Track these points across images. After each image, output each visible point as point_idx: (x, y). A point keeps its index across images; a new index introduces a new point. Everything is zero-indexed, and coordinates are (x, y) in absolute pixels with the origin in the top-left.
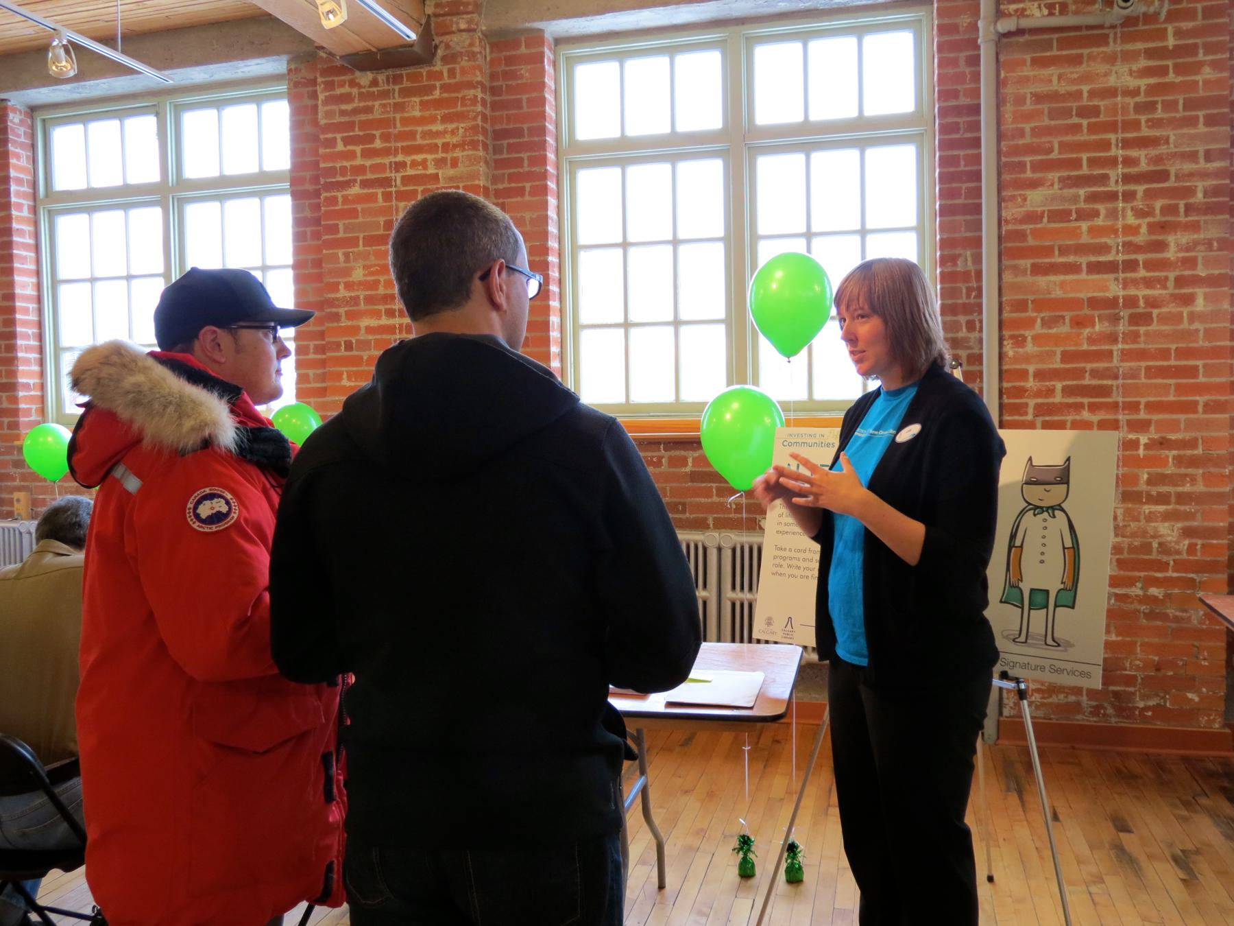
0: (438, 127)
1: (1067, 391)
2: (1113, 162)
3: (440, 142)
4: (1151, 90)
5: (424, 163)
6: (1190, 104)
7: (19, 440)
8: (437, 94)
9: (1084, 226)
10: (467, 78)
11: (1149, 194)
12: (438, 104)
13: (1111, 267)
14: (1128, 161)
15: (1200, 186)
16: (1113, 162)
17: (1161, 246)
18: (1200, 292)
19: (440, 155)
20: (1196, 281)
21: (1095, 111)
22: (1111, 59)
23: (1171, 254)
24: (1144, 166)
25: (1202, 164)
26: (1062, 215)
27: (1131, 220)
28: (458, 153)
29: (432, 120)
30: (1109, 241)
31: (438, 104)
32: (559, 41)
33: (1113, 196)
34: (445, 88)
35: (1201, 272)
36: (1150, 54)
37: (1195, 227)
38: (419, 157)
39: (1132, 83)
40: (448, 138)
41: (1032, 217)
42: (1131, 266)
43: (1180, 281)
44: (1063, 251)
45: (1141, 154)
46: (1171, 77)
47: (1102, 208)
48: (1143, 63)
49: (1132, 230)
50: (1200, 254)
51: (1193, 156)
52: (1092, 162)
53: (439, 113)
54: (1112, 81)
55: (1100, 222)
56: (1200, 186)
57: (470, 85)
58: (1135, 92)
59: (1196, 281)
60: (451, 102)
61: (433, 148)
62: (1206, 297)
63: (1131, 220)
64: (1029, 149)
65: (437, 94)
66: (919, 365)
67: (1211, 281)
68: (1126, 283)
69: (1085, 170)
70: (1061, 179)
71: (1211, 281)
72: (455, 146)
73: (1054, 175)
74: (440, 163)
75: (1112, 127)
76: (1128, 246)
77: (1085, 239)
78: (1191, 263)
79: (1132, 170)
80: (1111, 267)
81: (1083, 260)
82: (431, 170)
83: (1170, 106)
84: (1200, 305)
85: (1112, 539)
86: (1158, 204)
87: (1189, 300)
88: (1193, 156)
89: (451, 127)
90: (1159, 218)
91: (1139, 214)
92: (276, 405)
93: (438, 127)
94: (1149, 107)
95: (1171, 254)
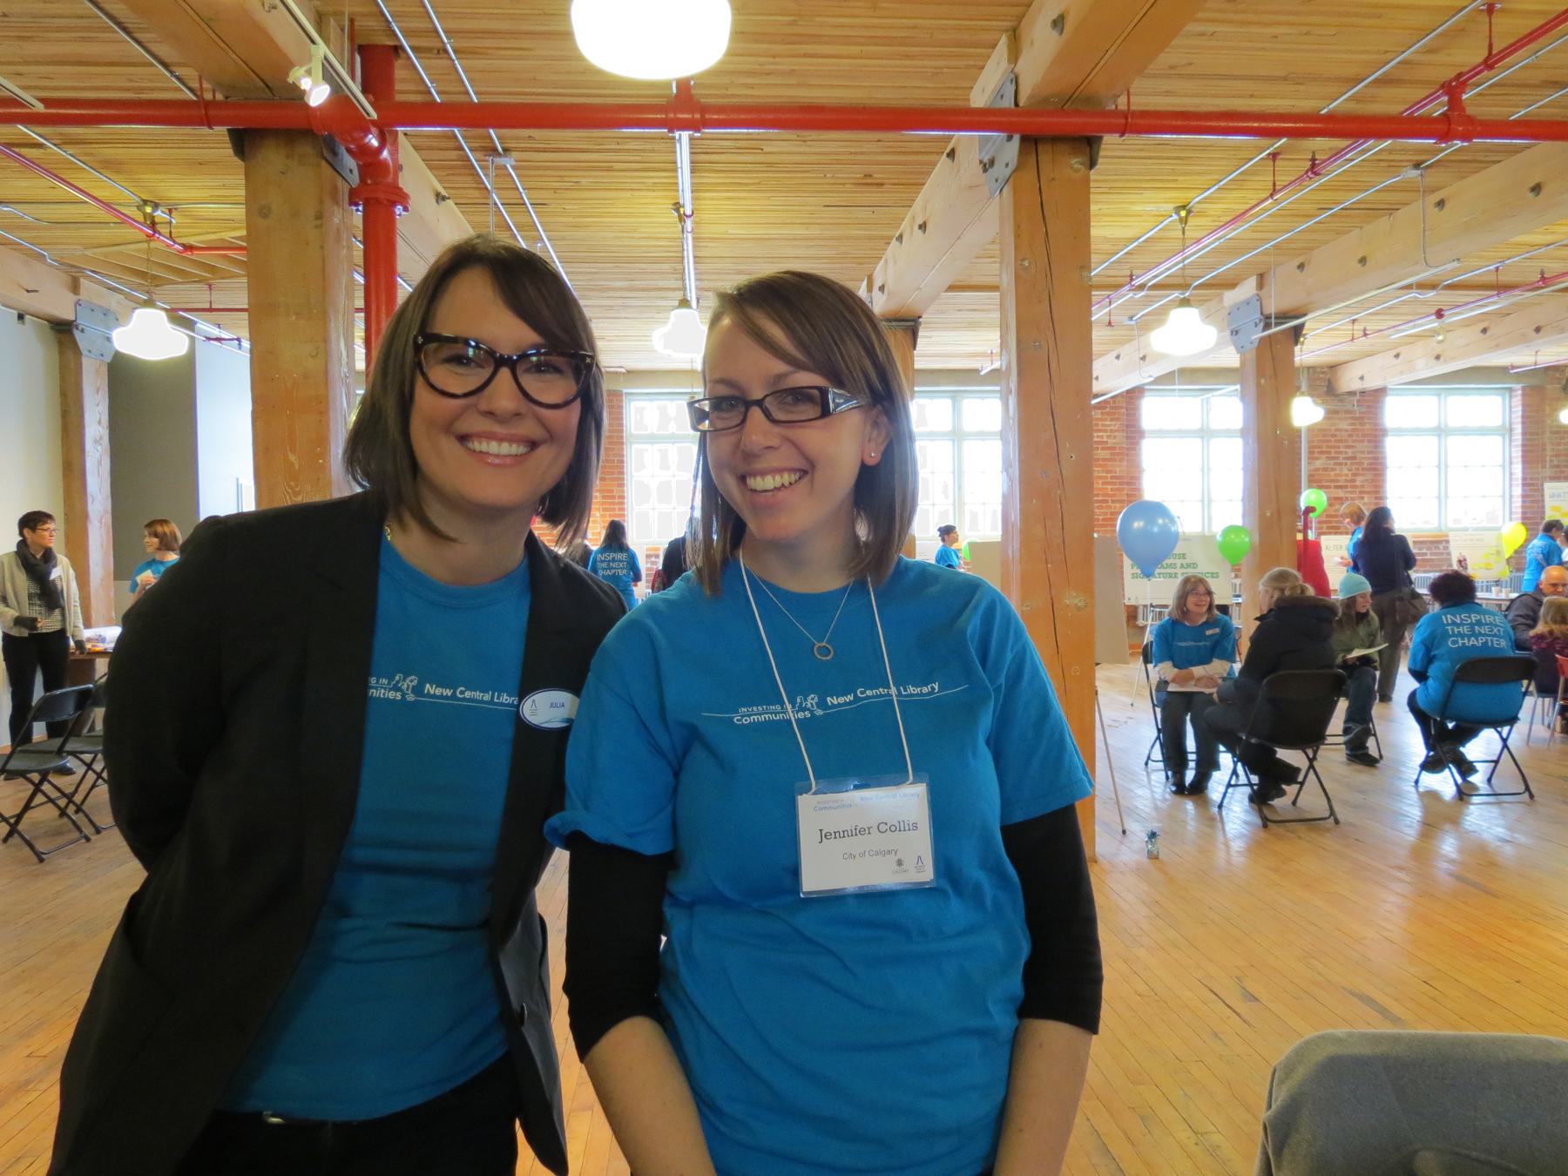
0: (1107, 423)
1: (1328, 528)
2: (1340, 453)
3: (1109, 428)
4: (1353, 430)
5: (1102, 436)
6: (1364, 435)
7: (1215, 536)
8: (1108, 410)
9: (1333, 473)
10: (1121, 405)
11: (1352, 464)
12: (1107, 414)
13: (1340, 487)
14: (1346, 453)
15: (1366, 462)
16: (1340, 453)
17: (1354, 481)
18: (1366, 496)
19: (1109, 434)
20: (1364, 492)
21: (1335, 436)
22: (1340, 419)
23: (1358, 483)
24: (1350, 455)
25: (1366, 455)
26: (1325, 469)
27: (1347, 472)
28: (1116, 434)
29: (1106, 420)
30: (1340, 478)
31: (1107, 414)
32: (626, 393)
33: (1341, 464)
34: (1112, 408)
35: (1367, 490)
36: (1351, 418)
37: (1363, 475)
38: (1100, 434)
39: (1346, 427)
40: (1112, 428)
41: (1318, 470)
42: (1346, 486)
43: (1360, 492)
44: (1327, 481)
45: (1349, 451)
46: (1358, 427)
47: (1338, 467)
48: (1350, 421)
49: (1347, 475)
50: (1366, 484)
51: (1363, 452)
52: (1336, 452)
53: (1108, 417)
54: (1340, 426)
55: (1337, 472)
56: (1366, 462)
57: (1121, 408)
58: (1346, 431)
59: (1364, 492)
60: (1114, 414)
61: (1106, 431)
62: (1368, 498)
63: (1347, 472)
64: (1333, 447)
65: (1108, 410)
66: (39, 527)
67: (1368, 493)
68: (1346, 492)
69: (1333, 455)
70: (1326, 457)
71: (1368, 493)
72: (1115, 431)
73: (1324, 456)
74: (1108, 437)
75: (1341, 441)
76: (1346, 481)
77: (1333, 478)
78: (1363, 486)
79: (1346, 456)
80: (1340, 487)
81: (1333, 484)
82: (1105, 439)
83: (1358, 435)
84: (1366, 500)
85: (1139, 579)
86: (1354, 467)
87: (1363, 498)
88: (1363, 452)
89: (1113, 423)
90: (1354, 472)
91: (1349, 470)
92: (179, 534)
93: (1107, 423)
94: (1350, 436)
95: (1358, 483)
